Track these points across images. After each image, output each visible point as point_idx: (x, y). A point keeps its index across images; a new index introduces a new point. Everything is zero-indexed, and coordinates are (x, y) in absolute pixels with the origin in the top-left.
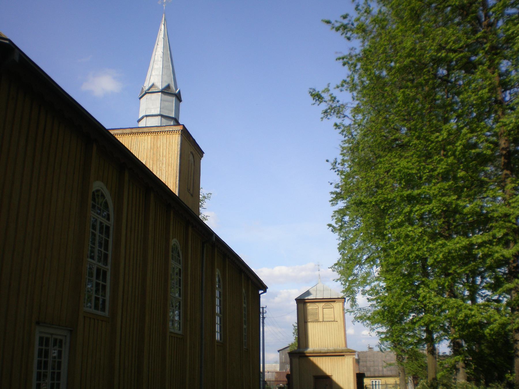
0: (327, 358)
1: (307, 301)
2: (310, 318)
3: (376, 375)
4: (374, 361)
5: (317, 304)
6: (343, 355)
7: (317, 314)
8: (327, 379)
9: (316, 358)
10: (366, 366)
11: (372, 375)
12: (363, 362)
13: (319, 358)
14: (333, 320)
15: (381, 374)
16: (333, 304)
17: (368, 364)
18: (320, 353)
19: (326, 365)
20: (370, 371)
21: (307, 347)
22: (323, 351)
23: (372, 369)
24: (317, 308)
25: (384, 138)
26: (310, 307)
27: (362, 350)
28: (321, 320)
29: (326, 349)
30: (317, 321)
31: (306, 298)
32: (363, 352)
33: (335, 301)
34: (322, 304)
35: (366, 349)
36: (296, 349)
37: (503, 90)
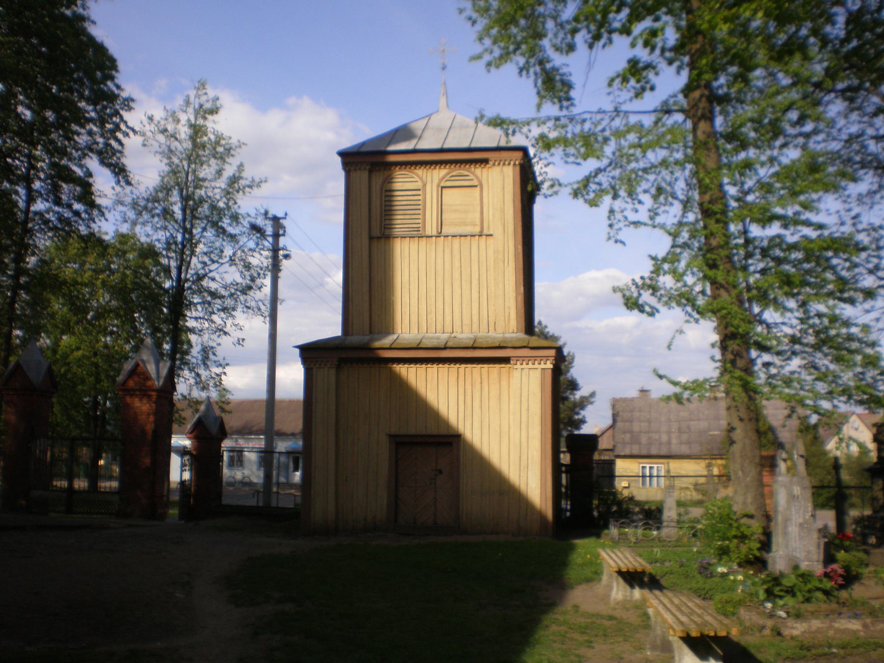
0: (444, 369)
1: (392, 158)
2: (401, 222)
3: (654, 452)
4: (649, 421)
5: (420, 171)
6: (506, 360)
7: (419, 208)
8: (448, 443)
9: (421, 369)
10: (631, 432)
11: (644, 452)
12: (623, 421)
13: (433, 369)
14: (477, 230)
15: (664, 452)
16: (478, 171)
17: (636, 427)
18: (417, 348)
19: (443, 392)
20: (640, 444)
21: (388, 330)
22: (427, 343)
23: (644, 439)
24: (419, 185)
25: (724, 478)
26: (404, 182)
27: (624, 396)
28: (431, 228)
29: (445, 336)
30: (419, 235)
31: (392, 148)
32: (625, 400)
33: (485, 161)
34: (437, 175)
35: (633, 393)
36: (339, 333)
37: (846, 65)
